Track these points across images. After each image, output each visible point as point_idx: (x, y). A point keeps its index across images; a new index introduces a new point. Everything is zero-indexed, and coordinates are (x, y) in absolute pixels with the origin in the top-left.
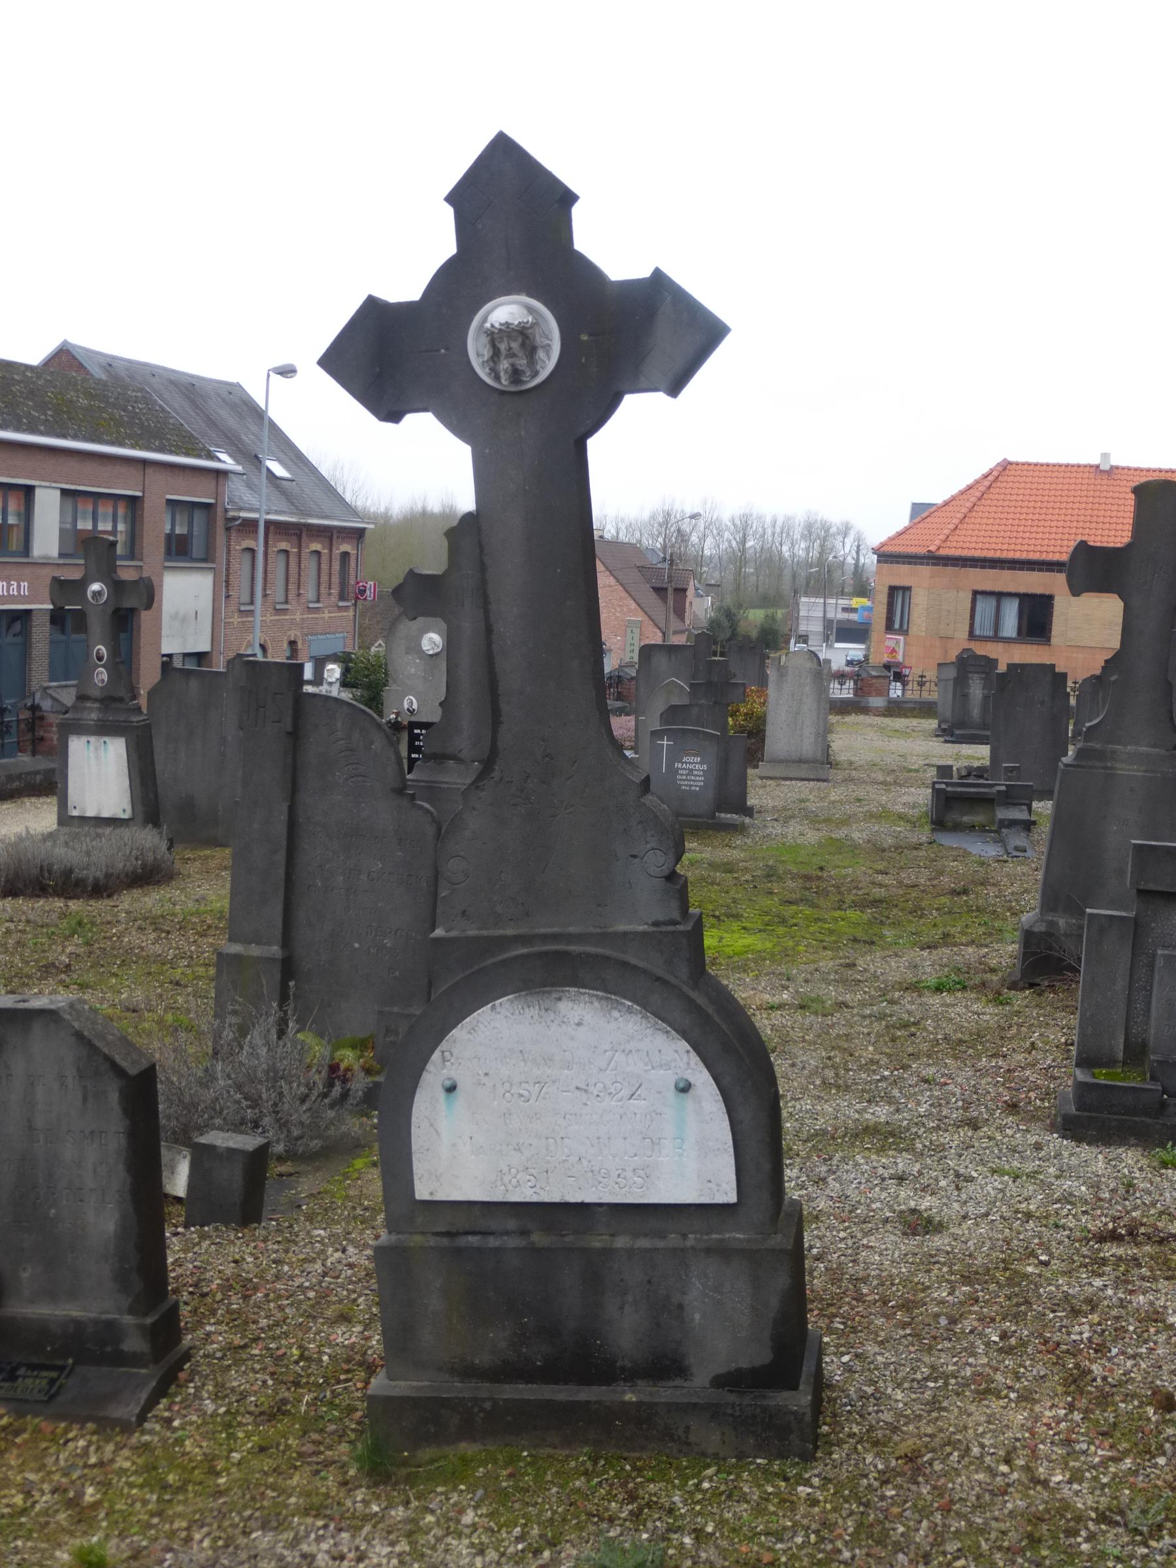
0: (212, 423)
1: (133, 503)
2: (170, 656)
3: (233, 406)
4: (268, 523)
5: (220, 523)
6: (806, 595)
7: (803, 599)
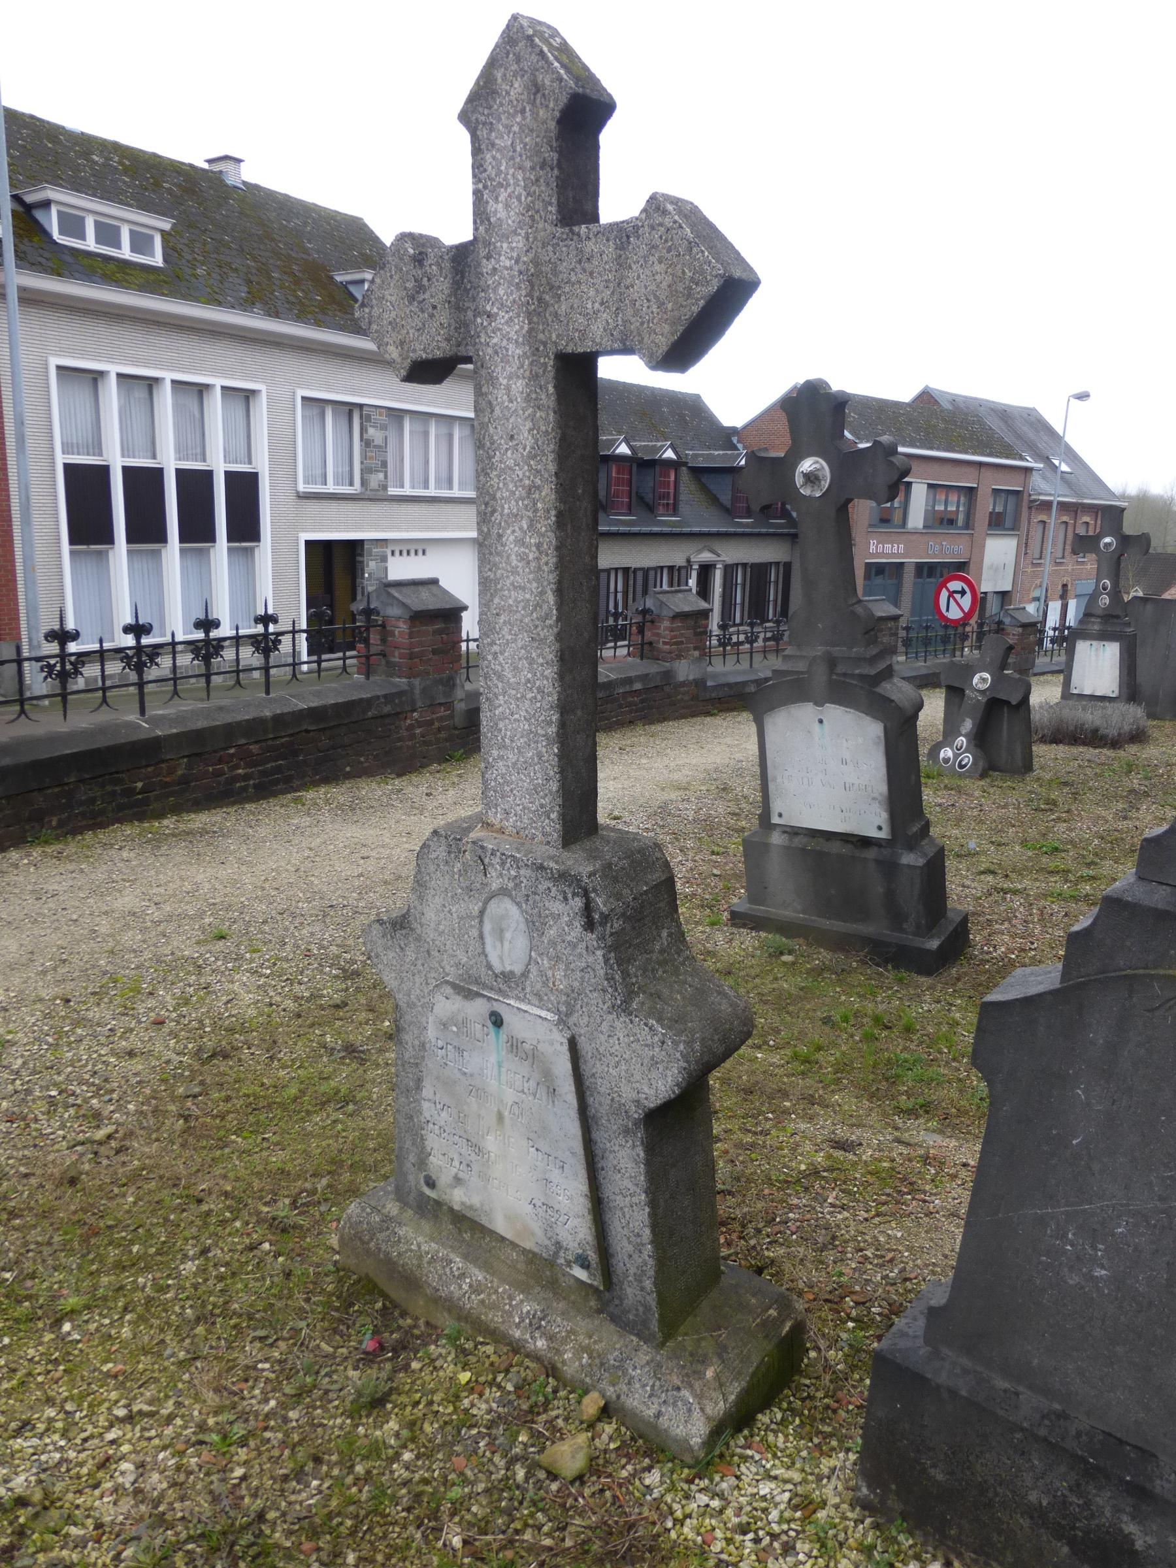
0: (1019, 437)
1: (971, 491)
2: (985, 593)
3: (1031, 424)
4: (1059, 503)
5: (1025, 504)
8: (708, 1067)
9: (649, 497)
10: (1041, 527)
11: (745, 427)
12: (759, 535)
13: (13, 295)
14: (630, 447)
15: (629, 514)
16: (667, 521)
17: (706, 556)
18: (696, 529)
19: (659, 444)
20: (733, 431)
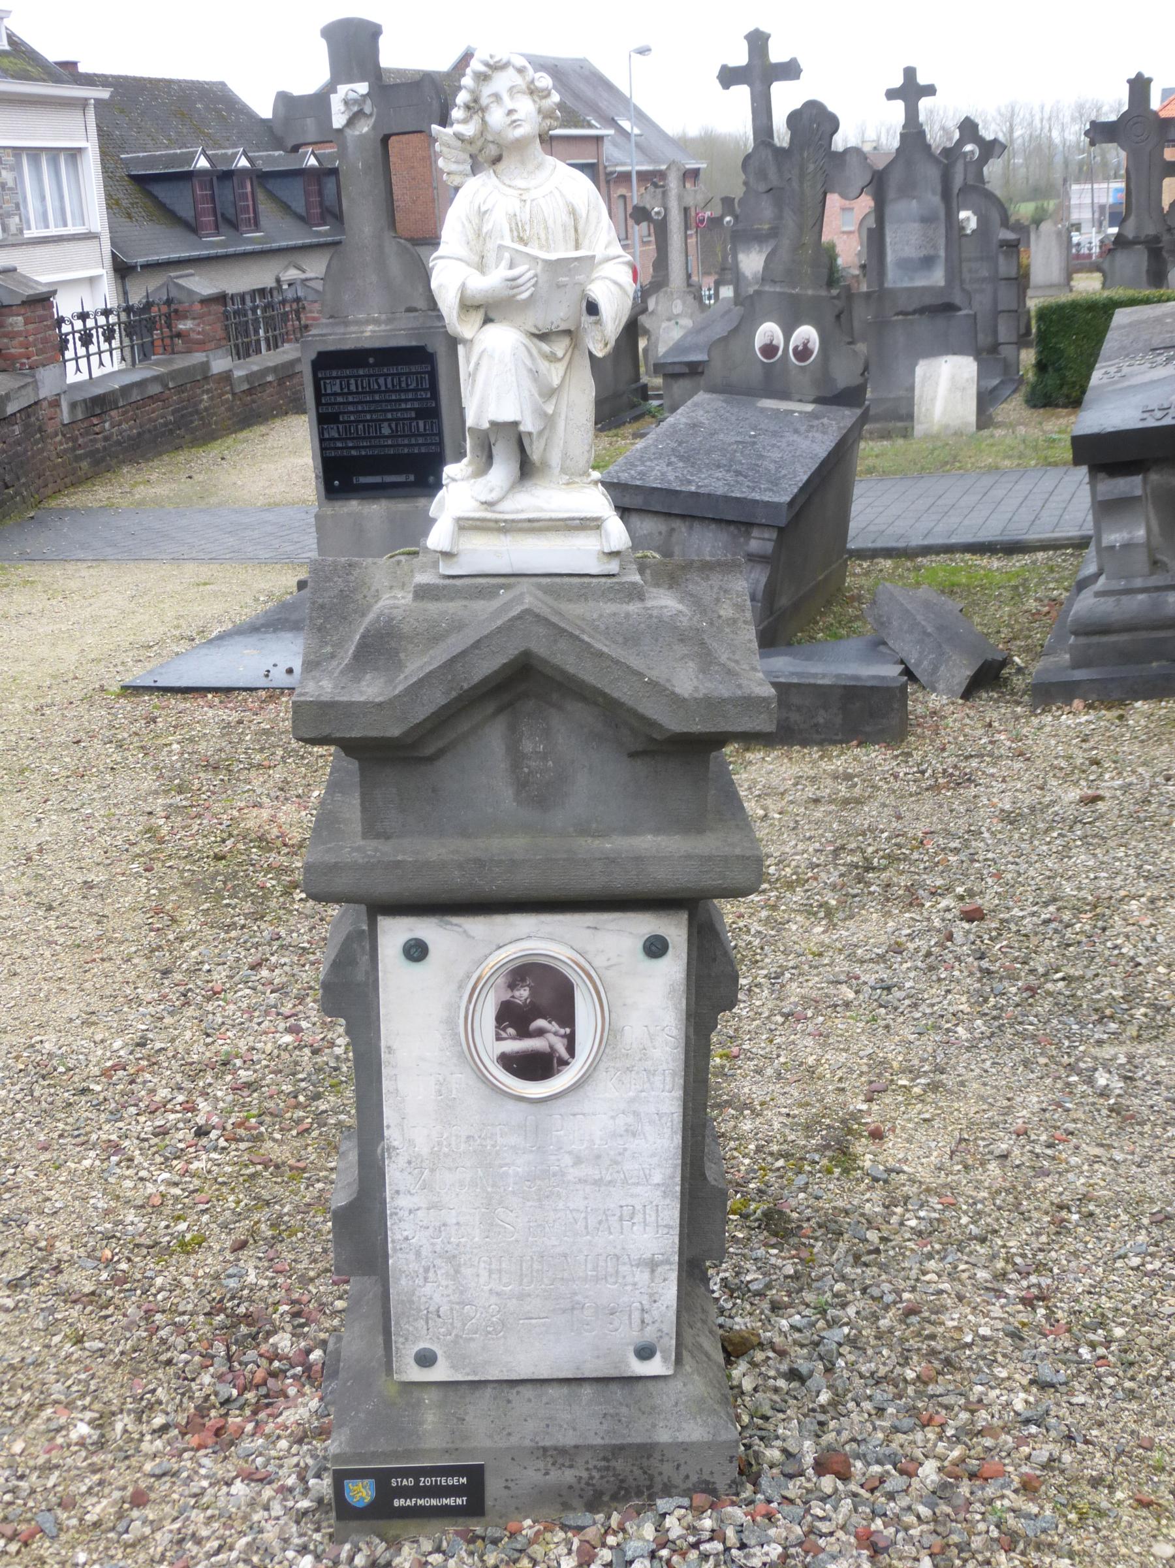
4: (639, 173)
6: (1078, 181)
7: (1075, 187)
8: (735, 331)
9: (230, 213)
10: (621, 202)
12: (226, 257)
14: (249, 159)
15: (218, 235)
16: (253, 239)
18: (284, 244)
19: (230, 151)
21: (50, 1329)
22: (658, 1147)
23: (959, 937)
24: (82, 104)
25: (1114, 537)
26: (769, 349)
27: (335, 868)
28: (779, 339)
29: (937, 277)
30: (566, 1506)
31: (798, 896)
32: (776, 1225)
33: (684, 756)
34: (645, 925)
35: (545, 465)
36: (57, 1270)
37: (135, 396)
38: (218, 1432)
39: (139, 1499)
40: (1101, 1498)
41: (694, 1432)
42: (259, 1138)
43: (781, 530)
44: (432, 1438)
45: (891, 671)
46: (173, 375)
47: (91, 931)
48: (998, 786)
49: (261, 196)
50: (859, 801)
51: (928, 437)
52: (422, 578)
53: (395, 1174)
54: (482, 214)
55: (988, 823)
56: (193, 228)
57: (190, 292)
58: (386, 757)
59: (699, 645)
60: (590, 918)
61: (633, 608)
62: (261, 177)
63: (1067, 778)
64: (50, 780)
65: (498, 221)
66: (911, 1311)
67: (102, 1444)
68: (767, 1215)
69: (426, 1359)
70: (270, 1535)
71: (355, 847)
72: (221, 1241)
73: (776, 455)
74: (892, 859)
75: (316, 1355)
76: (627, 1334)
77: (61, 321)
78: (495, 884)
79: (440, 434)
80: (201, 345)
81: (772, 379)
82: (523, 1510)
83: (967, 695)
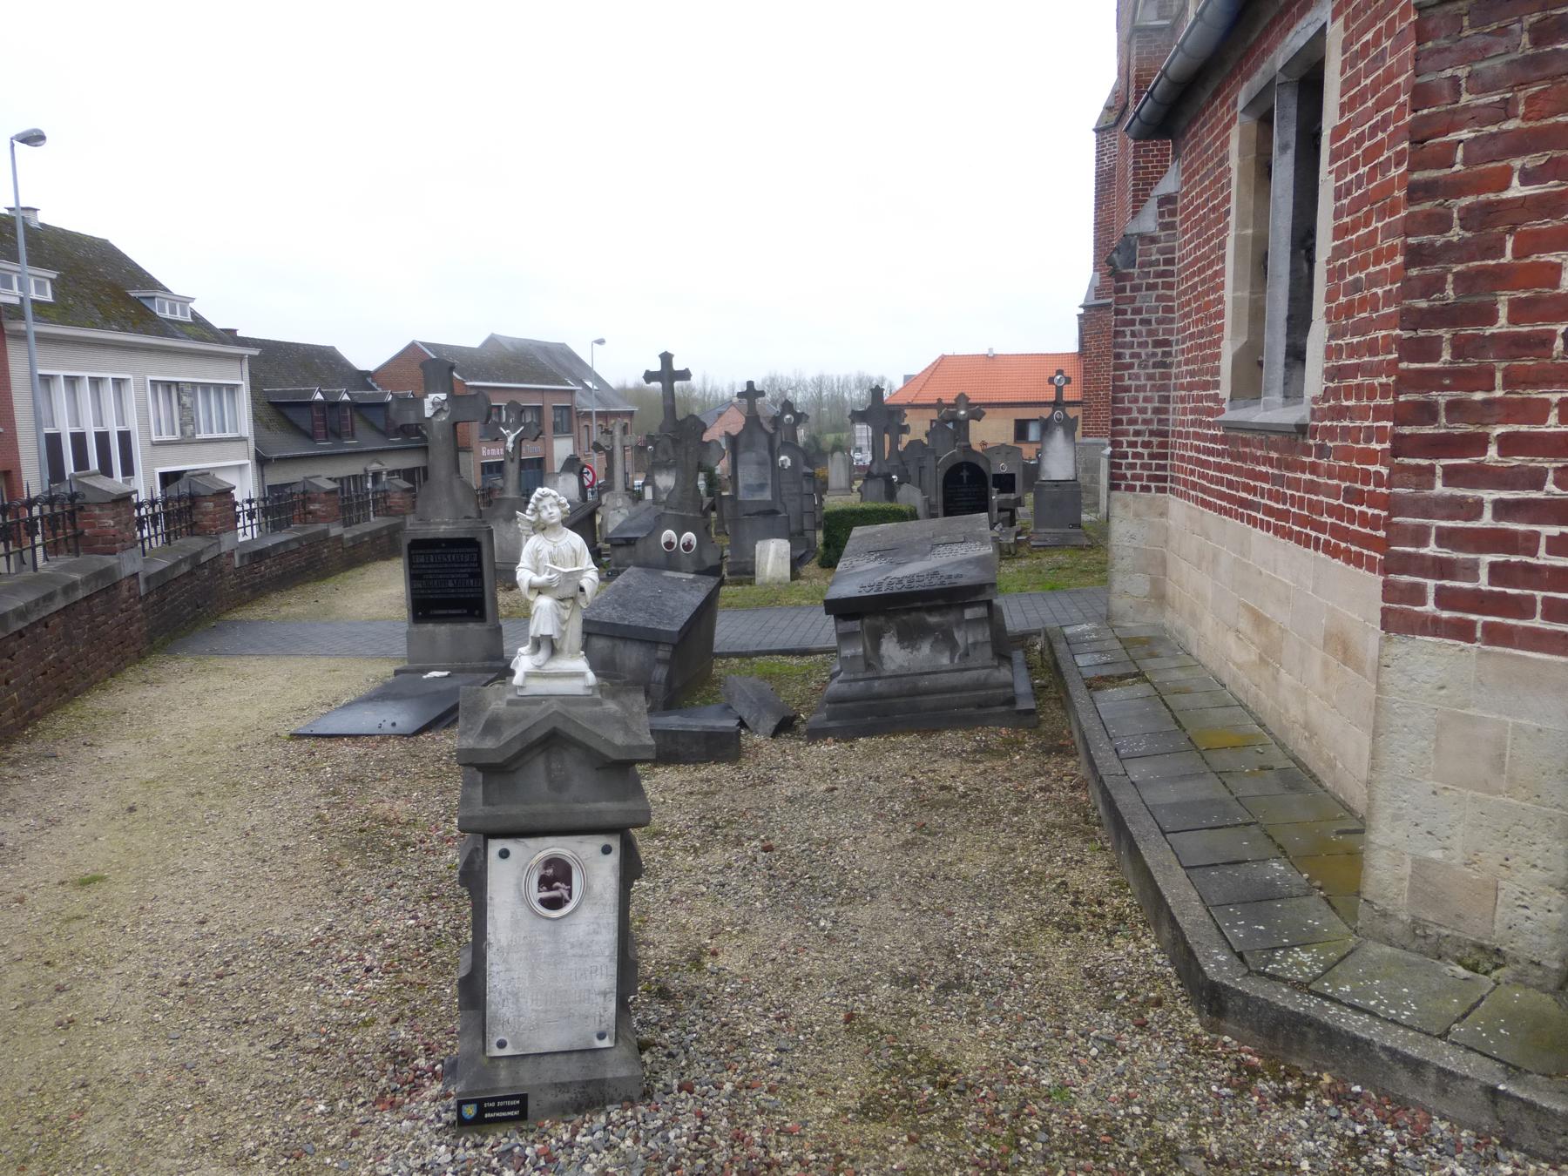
11: (376, 371)
13: (32, 337)
17: (375, 467)
20: (368, 373)
21: (297, 1066)
22: (607, 939)
23: (759, 859)
24: (240, 358)
25: (847, 652)
26: (669, 544)
27: (472, 818)
28: (675, 539)
29: (767, 495)
30: (565, 1113)
31: (680, 842)
32: (664, 994)
33: (619, 770)
34: (602, 840)
35: (561, 650)
36: (297, 1039)
37: (282, 550)
38: (392, 1103)
39: (355, 1133)
40: (803, 1093)
41: (623, 1072)
42: (400, 971)
43: (675, 646)
44: (504, 1081)
45: (732, 723)
46: (306, 537)
47: (291, 873)
48: (785, 784)
49: (356, 418)
50: (713, 793)
51: (764, 584)
52: (511, 696)
53: (491, 956)
54: (538, 551)
55: (779, 803)
56: (310, 436)
57: (318, 487)
58: (493, 772)
59: (629, 724)
60: (579, 838)
61: (598, 709)
62: (356, 406)
63: (821, 779)
64: (252, 789)
65: (545, 553)
66: (724, 1025)
67: (332, 1113)
68: (660, 990)
69: (502, 1045)
70: (423, 1140)
71: (479, 809)
72: (384, 1020)
73: (672, 603)
74: (729, 822)
75: (438, 1067)
76: (593, 1027)
77: (236, 504)
78: (540, 824)
79: (482, 587)
80: (324, 519)
81: (671, 559)
82: (545, 1116)
83: (775, 734)
